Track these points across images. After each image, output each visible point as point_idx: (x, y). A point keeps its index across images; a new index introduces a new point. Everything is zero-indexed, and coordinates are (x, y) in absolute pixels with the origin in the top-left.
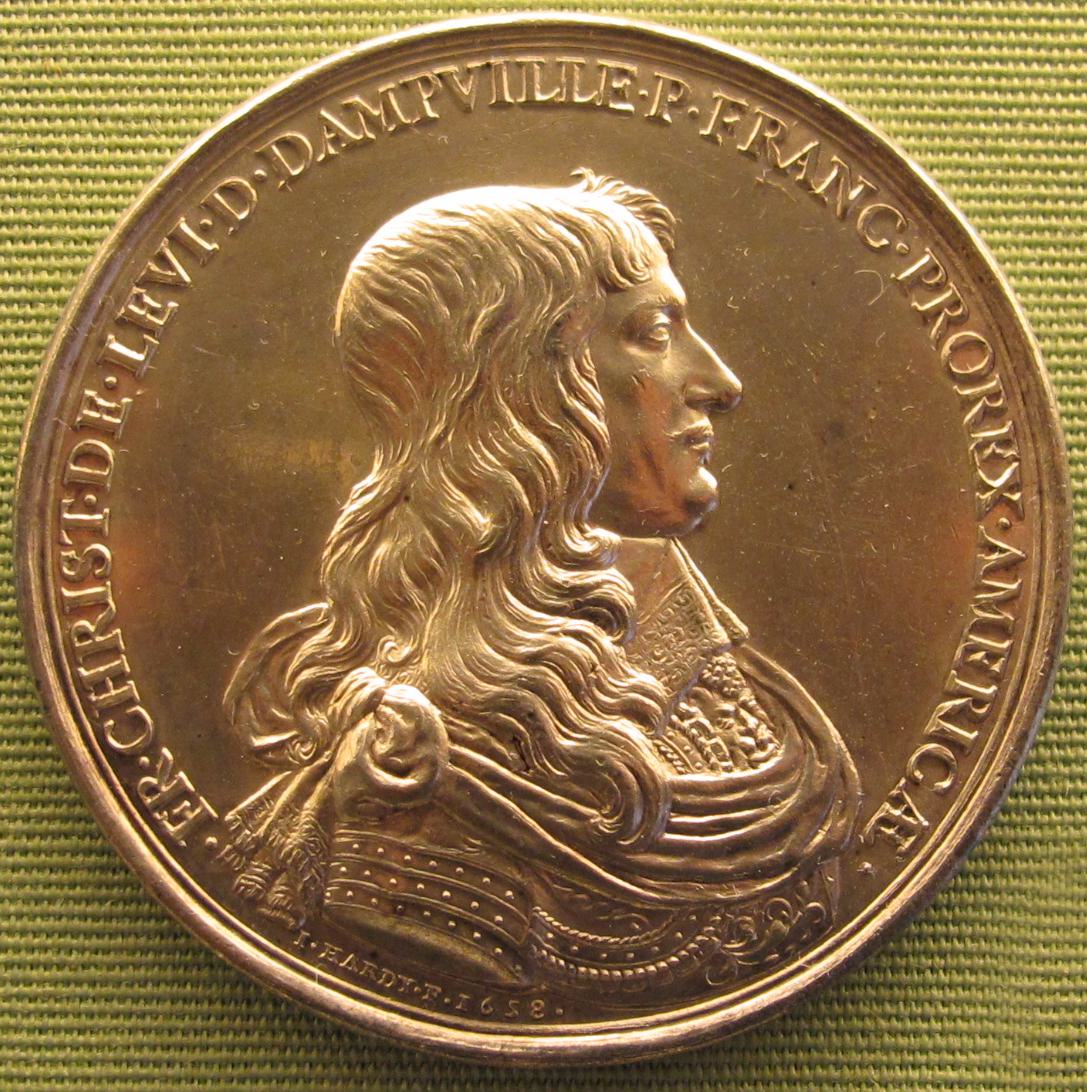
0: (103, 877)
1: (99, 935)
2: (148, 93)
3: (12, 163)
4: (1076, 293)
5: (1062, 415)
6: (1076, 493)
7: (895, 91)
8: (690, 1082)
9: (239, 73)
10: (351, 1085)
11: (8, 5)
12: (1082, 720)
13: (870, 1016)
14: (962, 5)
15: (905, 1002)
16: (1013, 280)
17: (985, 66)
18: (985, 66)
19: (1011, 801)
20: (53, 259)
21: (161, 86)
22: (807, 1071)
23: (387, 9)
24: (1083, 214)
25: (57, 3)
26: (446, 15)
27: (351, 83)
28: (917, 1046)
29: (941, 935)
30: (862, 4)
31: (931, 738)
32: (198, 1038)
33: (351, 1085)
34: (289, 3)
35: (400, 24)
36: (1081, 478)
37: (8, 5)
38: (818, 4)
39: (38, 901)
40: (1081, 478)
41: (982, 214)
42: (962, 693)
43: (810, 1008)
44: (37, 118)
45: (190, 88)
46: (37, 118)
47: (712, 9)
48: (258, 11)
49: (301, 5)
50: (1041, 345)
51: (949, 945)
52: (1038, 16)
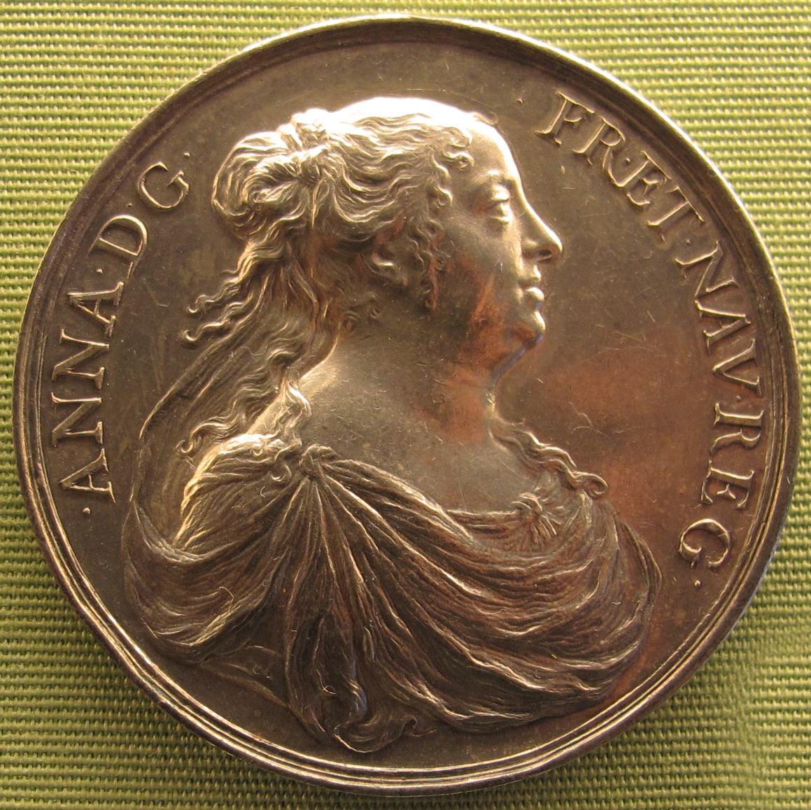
0: (29, 623)
2: (82, 58)
3: (115, 96)
7: (146, 89)
8: (551, 790)
9: (698, 47)
10: (188, 806)
11: (4, 6)
13: (721, 739)
15: (653, 776)
17: (636, 62)
18: (636, 62)
20: (16, 172)
22: (660, 780)
23: (265, 4)
24: (808, 603)
26: (358, 12)
29: (668, 729)
32: (11, 781)
33: (188, 806)
35: (326, 17)
41: (731, 171)
43: (625, 736)
44: (30, 74)
45: (32, 54)
46: (30, 74)
49: (319, 3)
51: (708, 802)
52: (141, 13)
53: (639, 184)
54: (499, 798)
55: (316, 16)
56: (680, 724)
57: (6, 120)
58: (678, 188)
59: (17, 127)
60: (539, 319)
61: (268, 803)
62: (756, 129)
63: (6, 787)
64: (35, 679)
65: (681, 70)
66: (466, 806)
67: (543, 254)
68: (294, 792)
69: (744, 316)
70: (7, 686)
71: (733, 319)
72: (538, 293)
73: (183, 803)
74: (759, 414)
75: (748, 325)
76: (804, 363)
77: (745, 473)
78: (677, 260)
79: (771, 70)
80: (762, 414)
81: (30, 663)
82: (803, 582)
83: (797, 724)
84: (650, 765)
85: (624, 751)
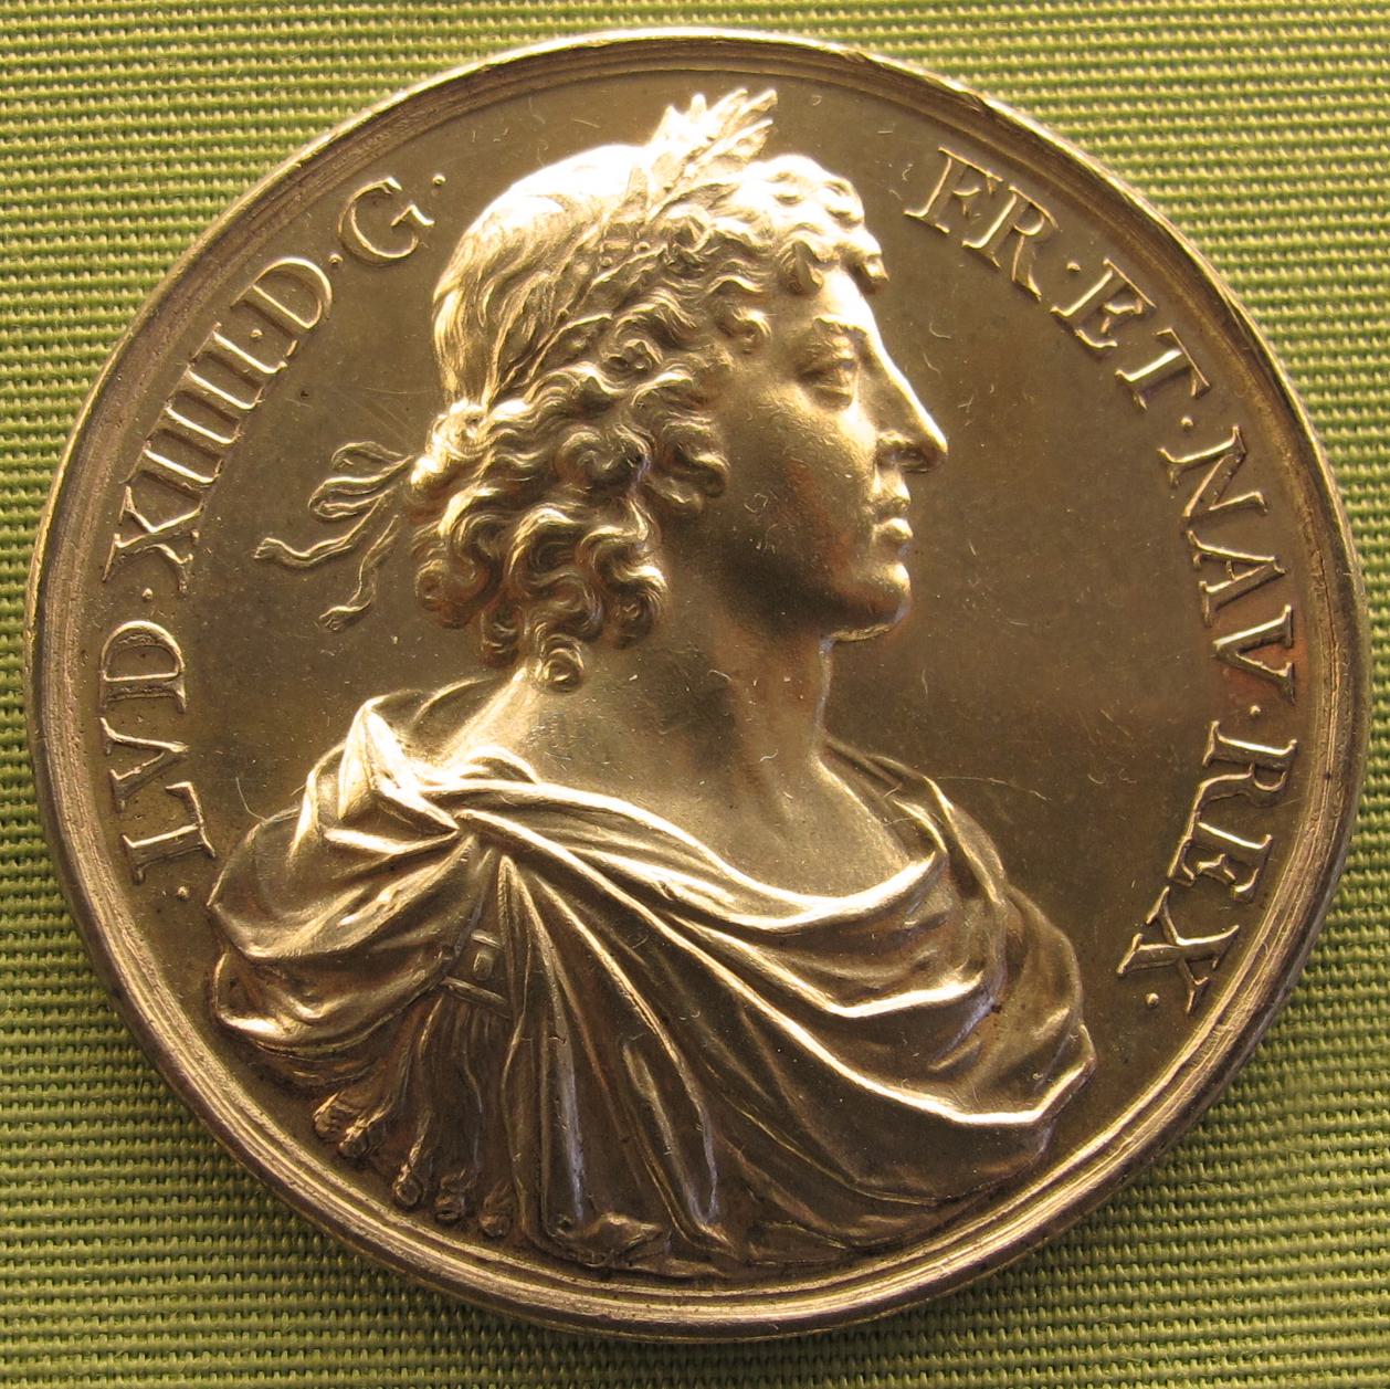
1: (44, 1122)
4: (1375, 1249)
5: (1344, 499)
6: (1376, 736)
12: (1382, 449)
14: (1091, 5)
16: (1265, 329)
19: (1300, 993)
21: (31, 98)
23: (159, 9)
25: (528, 5)
27: (634, 69)
28: (1198, 1255)
30: (599, 4)
31: (1217, 764)
34: (130, 4)
36: (1384, 718)
37: (7, 6)
38: (1230, 4)
39: (46, 1009)
40: (1384, 718)
41: (1261, 305)
42: (1239, 761)
47: (226, 8)
48: (94, 13)
50: (1313, 418)
53: (1095, 312)
54: (837, 1365)
55: (535, 33)
56: (1339, 1064)
57: (11, 351)
58: (1169, 330)
59: (20, 1299)
60: (899, 574)
61: (516, 1348)
62: (1363, 144)
63: (11, 1029)
64: (44, 1111)
65: (1173, 120)
66: (762, 1382)
67: (916, 459)
68: (481, 1328)
69: (1272, 559)
70: (11, 1029)
71: (1250, 565)
72: (902, 526)
73: (1133, 1382)
74: (1284, 746)
75: (1281, 575)
76: (1379, 643)
77: (1258, 838)
78: (1163, 451)
79: (1340, 116)
80: (1290, 747)
81: (109, 1278)
82: (1132, 1263)
83: (1317, 1296)
84: (1368, 1053)
85: (1072, 1260)
